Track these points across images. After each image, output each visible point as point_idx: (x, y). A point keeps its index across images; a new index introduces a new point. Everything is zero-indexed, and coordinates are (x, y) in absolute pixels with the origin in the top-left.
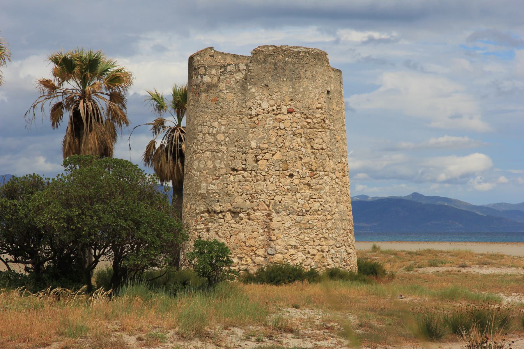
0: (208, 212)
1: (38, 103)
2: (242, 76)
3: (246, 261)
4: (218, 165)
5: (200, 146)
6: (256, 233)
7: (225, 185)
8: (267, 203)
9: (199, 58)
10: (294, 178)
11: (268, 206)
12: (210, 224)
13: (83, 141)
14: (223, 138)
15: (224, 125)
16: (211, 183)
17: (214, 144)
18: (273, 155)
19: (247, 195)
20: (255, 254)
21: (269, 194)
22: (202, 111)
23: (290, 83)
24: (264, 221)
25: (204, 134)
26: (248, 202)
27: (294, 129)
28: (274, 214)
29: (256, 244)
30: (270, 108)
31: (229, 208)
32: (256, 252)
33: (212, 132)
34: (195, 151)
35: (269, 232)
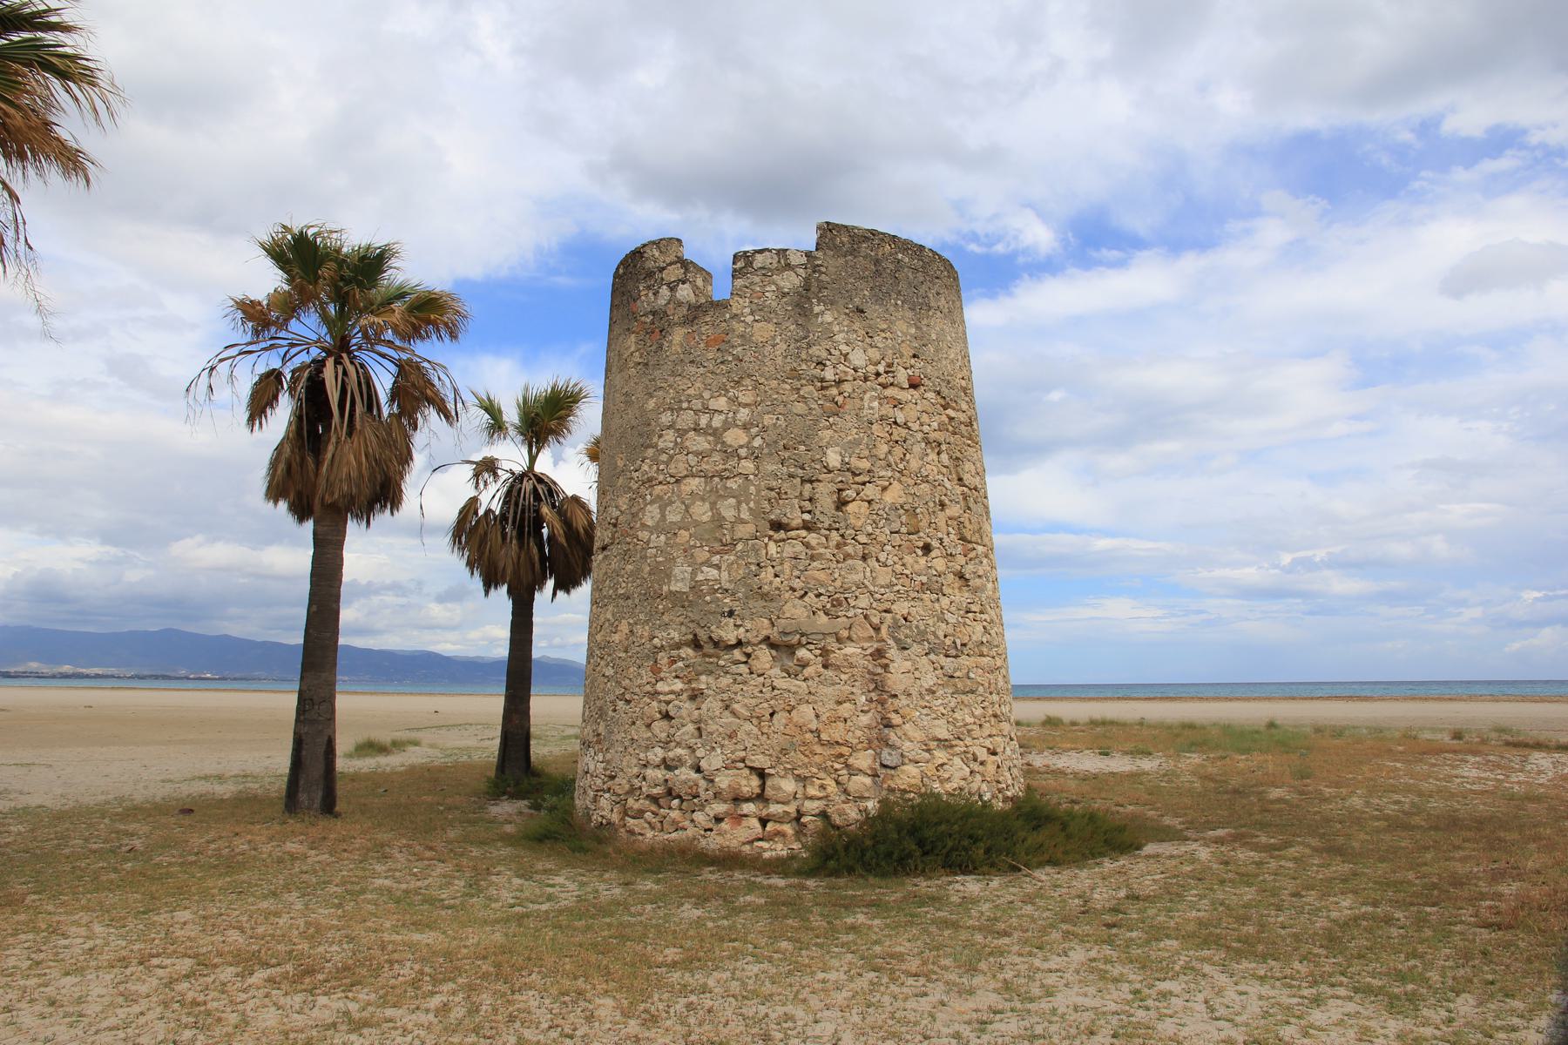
0: (696, 644)
1: (221, 360)
2: (797, 281)
3: (823, 787)
4: (729, 514)
5: (667, 464)
6: (847, 705)
7: (753, 568)
8: (876, 620)
9: (657, 254)
10: (933, 554)
11: (877, 629)
12: (703, 678)
13: (329, 455)
14: (744, 439)
15: (746, 405)
16: (708, 563)
17: (717, 457)
18: (884, 489)
19: (819, 595)
20: (847, 766)
21: (878, 596)
22: (673, 374)
23: (910, 314)
24: (869, 672)
25: (682, 433)
26: (823, 619)
27: (926, 428)
28: (893, 652)
29: (850, 737)
30: (871, 369)
31: (765, 633)
32: (851, 761)
33: (709, 425)
34: (650, 480)
35: (882, 703)
